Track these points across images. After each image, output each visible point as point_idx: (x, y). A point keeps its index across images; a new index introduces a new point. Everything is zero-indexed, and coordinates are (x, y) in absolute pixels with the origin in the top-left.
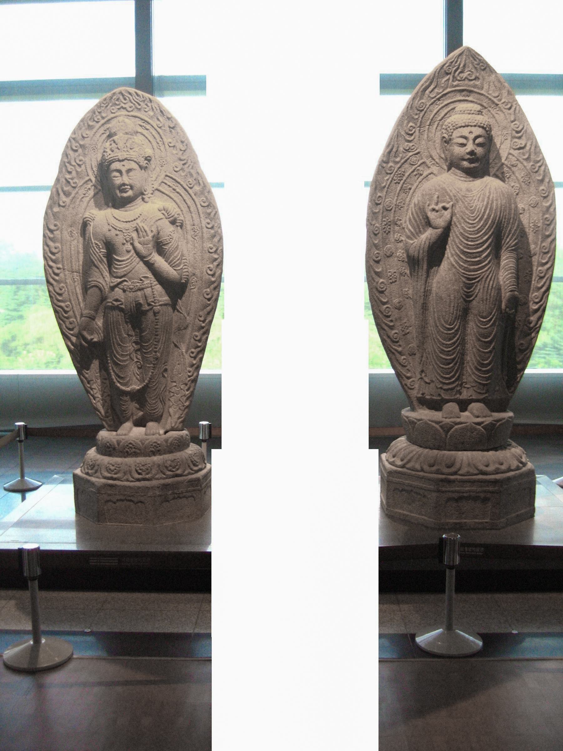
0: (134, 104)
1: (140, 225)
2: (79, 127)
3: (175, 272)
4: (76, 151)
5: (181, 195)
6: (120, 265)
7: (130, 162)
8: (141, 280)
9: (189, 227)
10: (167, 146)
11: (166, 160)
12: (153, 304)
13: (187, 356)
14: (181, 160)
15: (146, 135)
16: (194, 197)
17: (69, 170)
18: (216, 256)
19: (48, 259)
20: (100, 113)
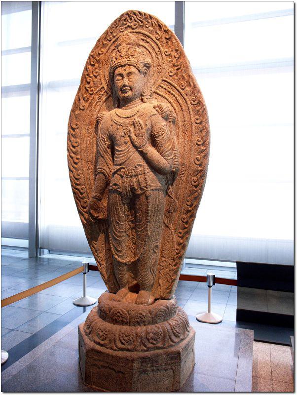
0: (138, 22)
1: (137, 119)
2: (96, 47)
3: (166, 162)
4: (93, 65)
5: (174, 96)
6: (119, 155)
7: (130, 66)
8: (136, 167)
9: (180, 124)
10: (164, 56)
11: (163, 67)
12: (145, 188)
13: (175, 236)
14: (175, 66)
15: (147, 47)
16: (186, 97)
17: (88, 81)
18: (203, 148)
19: (70, 151)
20: (111, 33)
